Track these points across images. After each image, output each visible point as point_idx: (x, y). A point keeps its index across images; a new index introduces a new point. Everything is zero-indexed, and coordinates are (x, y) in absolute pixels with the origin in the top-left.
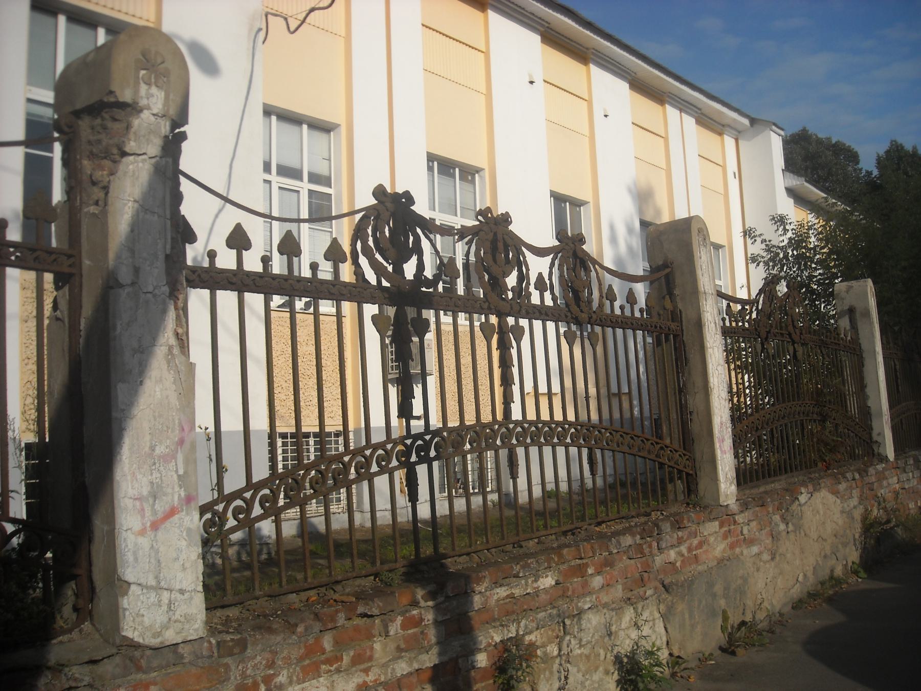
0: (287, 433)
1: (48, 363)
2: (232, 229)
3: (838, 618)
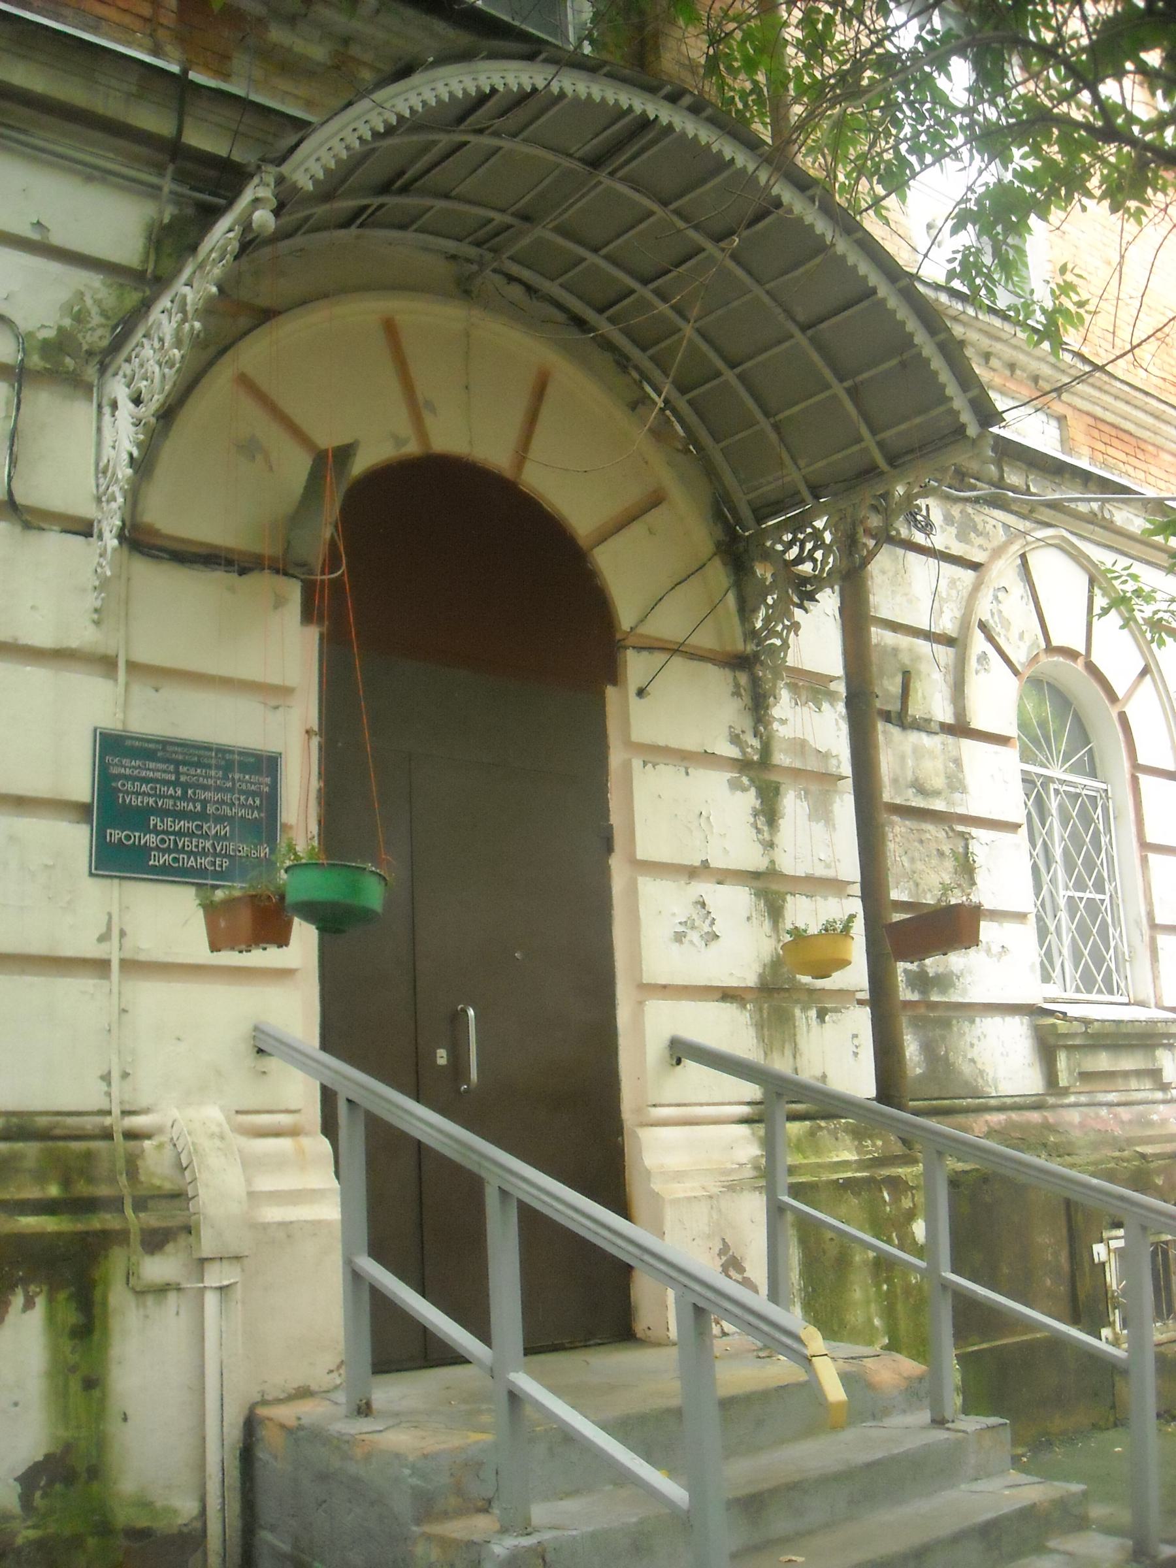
3: (1051, 1544)
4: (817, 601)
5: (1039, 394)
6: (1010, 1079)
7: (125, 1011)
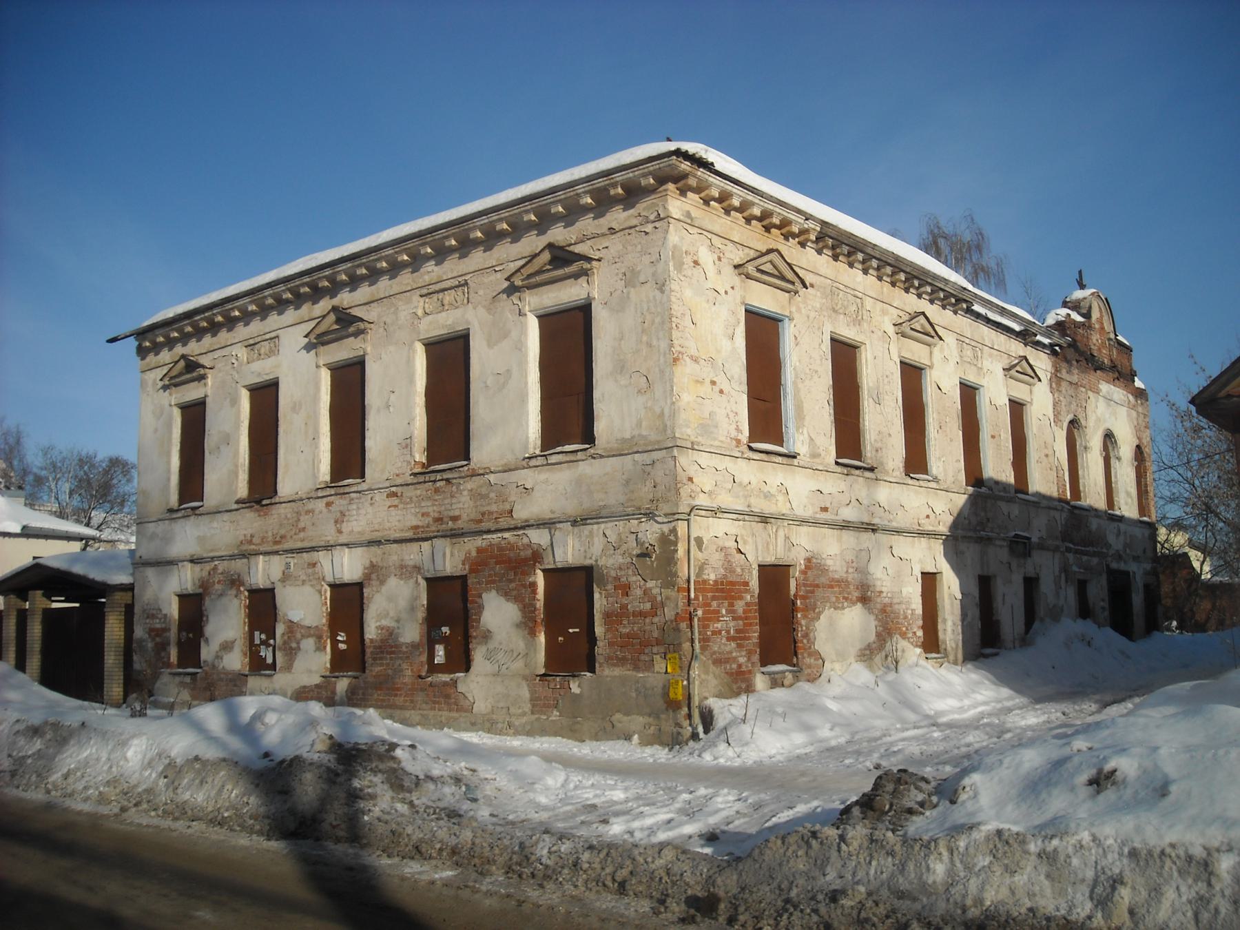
0: (1021, 646)
2: (920, 590)
5: (758, 254)
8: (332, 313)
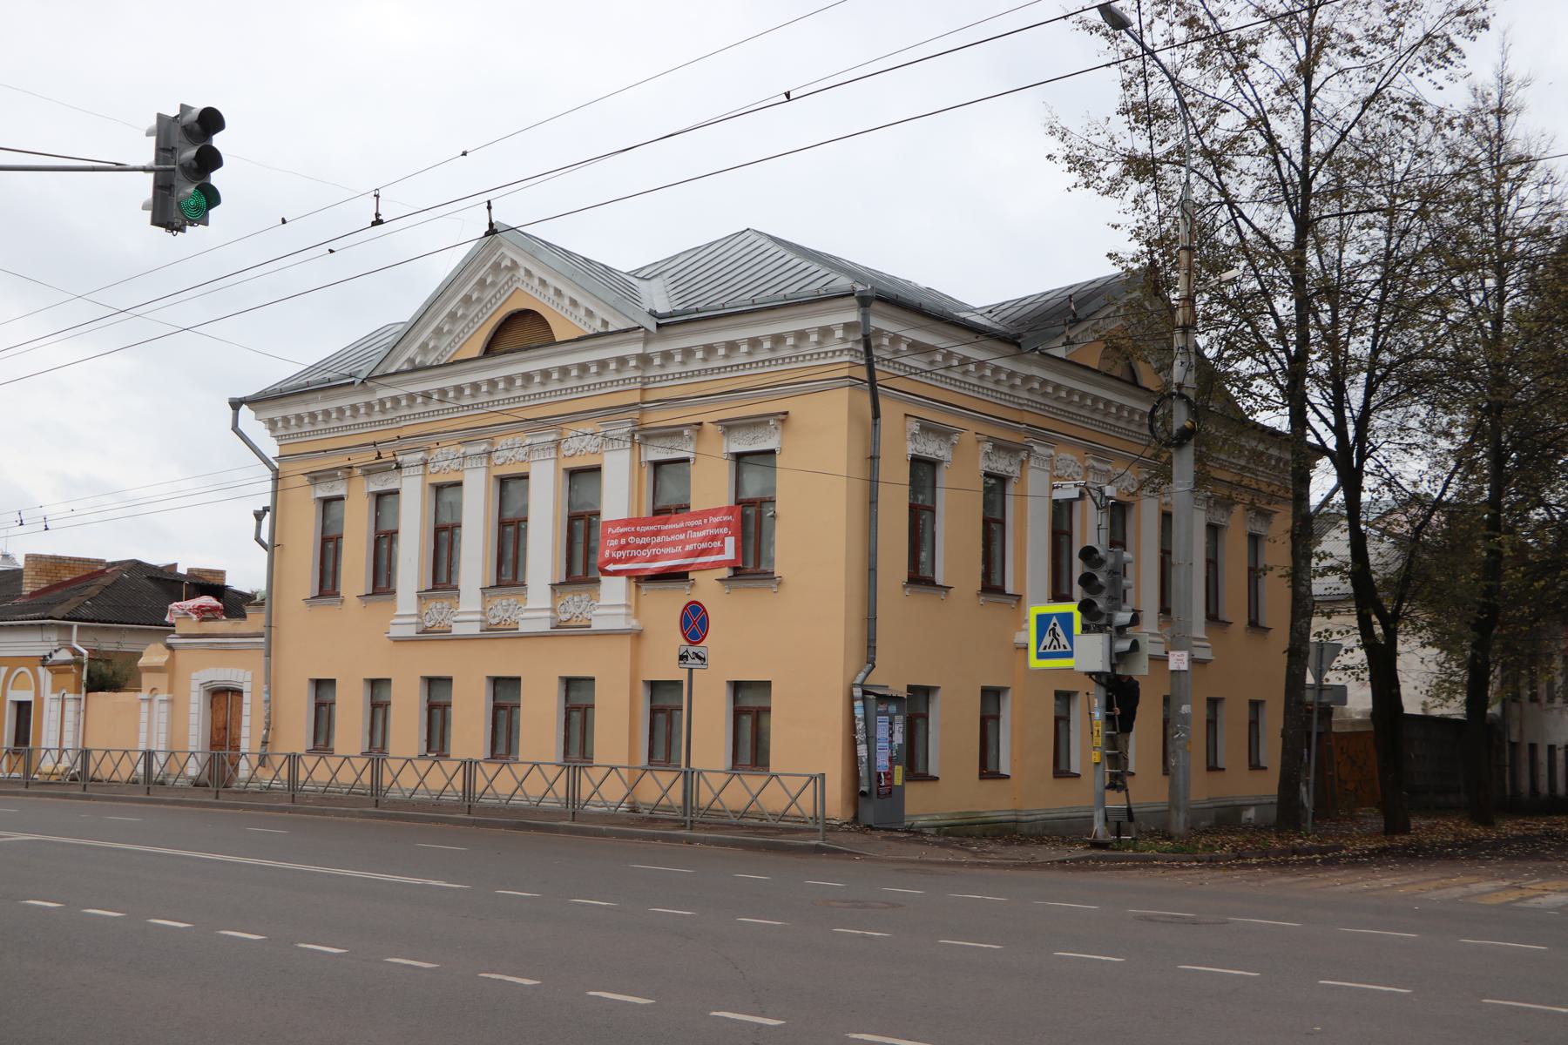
1: (37, 900)
4: (148, 134)
6: (1441, 88)
7: (284, 221)
8: (520, 760)
